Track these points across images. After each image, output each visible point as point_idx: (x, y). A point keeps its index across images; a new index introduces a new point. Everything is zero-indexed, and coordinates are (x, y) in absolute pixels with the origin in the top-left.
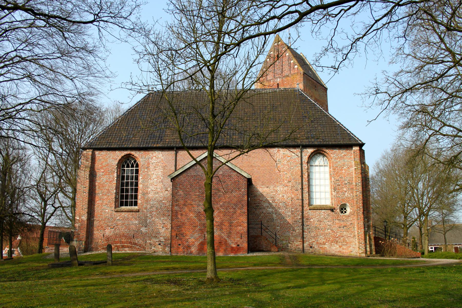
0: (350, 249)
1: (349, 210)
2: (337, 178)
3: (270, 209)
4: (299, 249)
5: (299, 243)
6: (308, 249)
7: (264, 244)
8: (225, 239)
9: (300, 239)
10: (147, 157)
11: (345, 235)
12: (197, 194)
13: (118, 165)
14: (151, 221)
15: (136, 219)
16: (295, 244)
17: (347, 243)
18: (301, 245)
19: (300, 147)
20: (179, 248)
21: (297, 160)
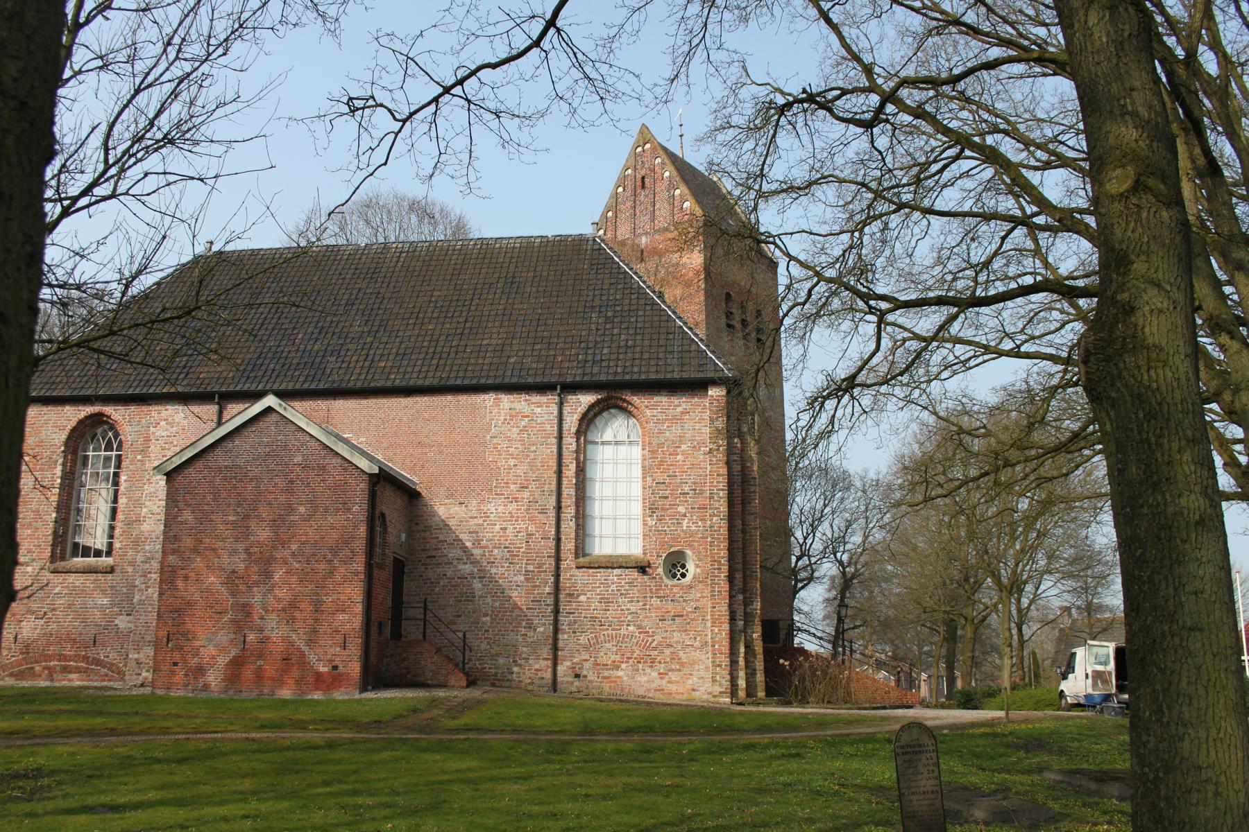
0: (690, 682)
1: (691, 568)
2: (660, 477)
3: (467, 566)
4: (544, 682)
5: (543, 664)
6: (568, 682)
7: (429, 663)
8: (299, 649)
9: (546, 651)
10: (144, 420)
11: (678, 642)
12: (231, 518)
13: (66, 443)
14: (144, 598)
15: (104, 592)
16: (530, 665)
17: (682, 664)
18: (550, 670)
19: (556, 389)
20: (173, 673)
21: (548, 427)
